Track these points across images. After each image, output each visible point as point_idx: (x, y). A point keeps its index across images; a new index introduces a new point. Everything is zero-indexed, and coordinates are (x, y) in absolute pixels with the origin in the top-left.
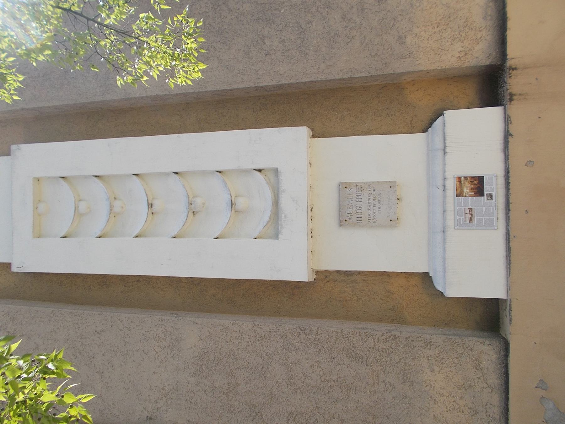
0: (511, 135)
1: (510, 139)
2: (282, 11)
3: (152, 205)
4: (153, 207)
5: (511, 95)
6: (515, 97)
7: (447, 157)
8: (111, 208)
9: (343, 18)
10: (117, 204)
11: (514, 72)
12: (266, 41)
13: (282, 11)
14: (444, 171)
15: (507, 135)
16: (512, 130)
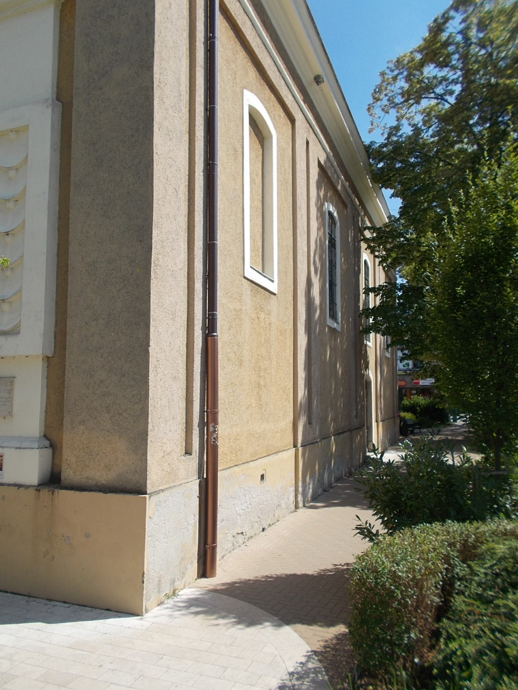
0: (19, 489)
1: (17, 488)
2: (113, 334)
3: (8, 235)
4: (6, 236)
5: (39, 490)
6: (38, 492)
7: (14, 450)
8: (8, 200)
9: (101, 381)
10: (11, 205)
11: (51, 493)
12: (95, 322)
13: (113, 334)
14: (7, 447)
15: (19, 486)
16: (22, 489)
